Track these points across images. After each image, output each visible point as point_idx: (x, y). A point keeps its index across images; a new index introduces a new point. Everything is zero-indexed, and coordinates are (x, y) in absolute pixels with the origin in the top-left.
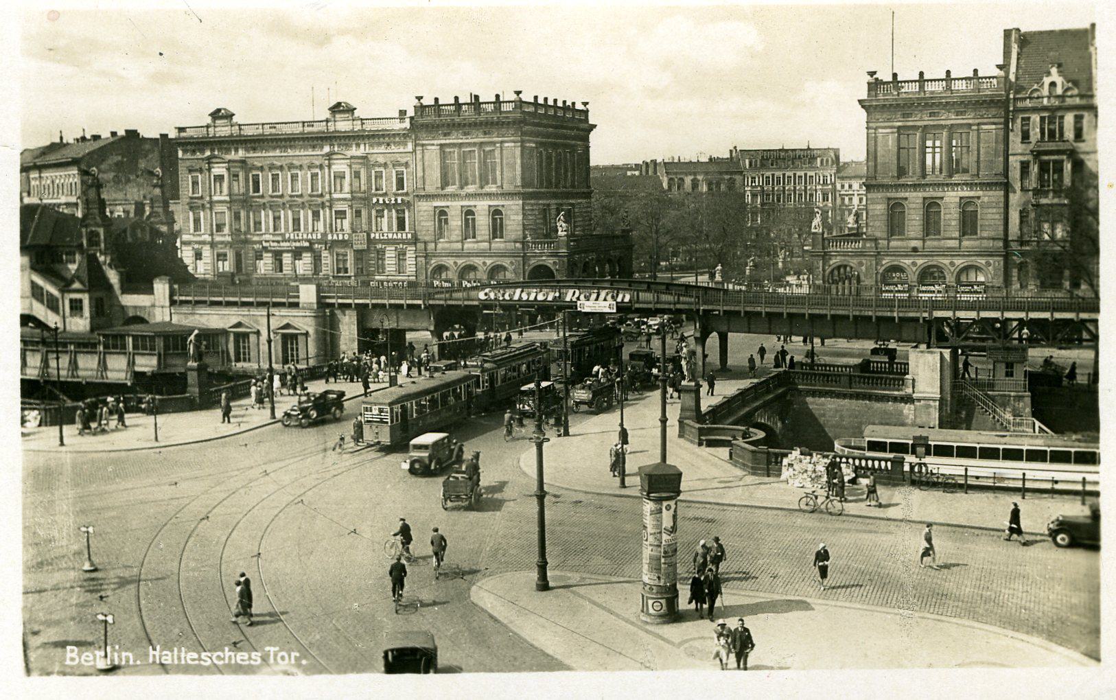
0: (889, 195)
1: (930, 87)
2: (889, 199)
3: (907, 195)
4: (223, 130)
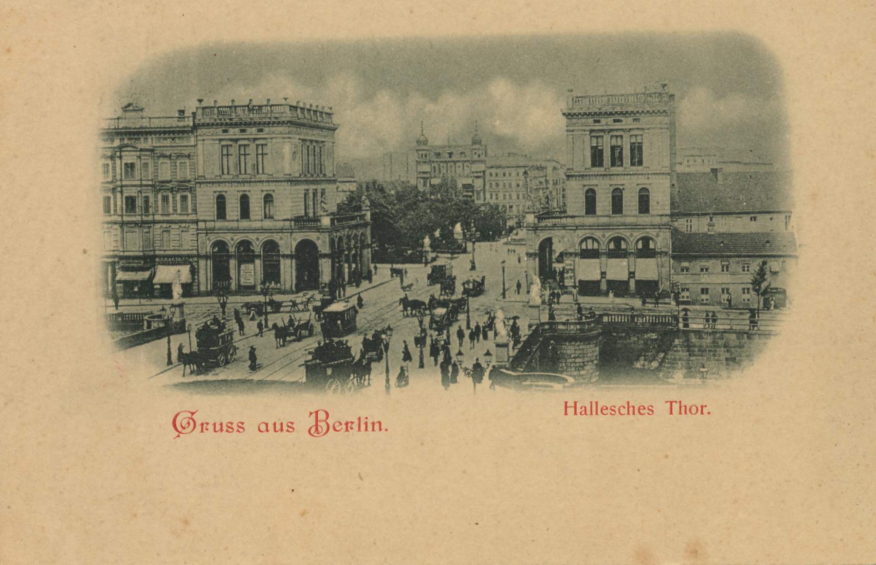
3: (225, 189)
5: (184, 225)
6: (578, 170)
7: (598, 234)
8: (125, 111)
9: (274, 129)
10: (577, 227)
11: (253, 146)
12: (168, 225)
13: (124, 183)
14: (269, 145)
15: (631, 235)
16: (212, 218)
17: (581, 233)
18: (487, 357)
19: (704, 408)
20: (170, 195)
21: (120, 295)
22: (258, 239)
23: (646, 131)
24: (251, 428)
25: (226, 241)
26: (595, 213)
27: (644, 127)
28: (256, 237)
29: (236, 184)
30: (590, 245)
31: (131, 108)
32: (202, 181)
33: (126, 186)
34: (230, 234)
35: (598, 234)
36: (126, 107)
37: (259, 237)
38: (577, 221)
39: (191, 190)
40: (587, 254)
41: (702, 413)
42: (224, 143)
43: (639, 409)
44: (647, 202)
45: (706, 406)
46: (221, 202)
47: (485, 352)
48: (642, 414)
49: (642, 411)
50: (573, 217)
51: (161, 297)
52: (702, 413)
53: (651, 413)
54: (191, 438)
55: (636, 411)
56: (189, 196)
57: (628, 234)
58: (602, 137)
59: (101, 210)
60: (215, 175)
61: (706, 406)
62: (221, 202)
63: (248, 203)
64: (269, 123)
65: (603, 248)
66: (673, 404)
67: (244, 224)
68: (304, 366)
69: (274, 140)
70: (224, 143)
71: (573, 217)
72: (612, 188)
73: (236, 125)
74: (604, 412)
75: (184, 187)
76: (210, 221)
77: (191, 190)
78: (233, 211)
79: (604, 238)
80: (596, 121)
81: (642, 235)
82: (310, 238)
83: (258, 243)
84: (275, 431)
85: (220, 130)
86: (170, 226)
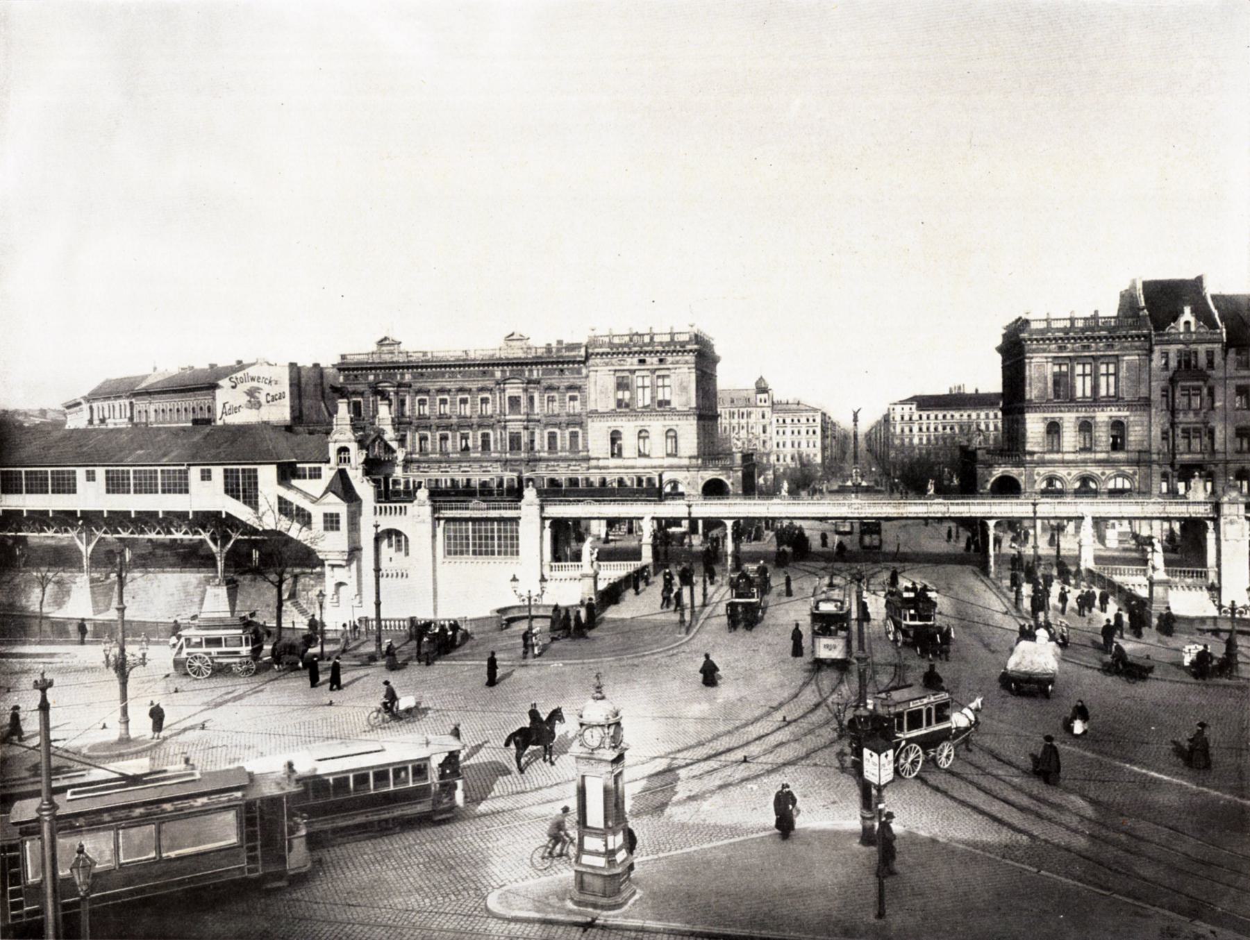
1: (1055, 325)
2: (1046, 418)
4: (517, 353)
8: (382, 345)
9: (678, 358)
13: (508, 418)
14: (673, 376)
16: (605, 456)
18: (514, 583)
20: (471, 434)
21: (1210, 524)
27: (671, 366)
31: (387, 342)
33: (509, 421)
36: (382, 341)
39: (581, 425)
42: (618, 374)
46: (615, 437)
47: (511, 577)
51: (572, 561)
56: (580, 432)
59: (623, 447)
62: (615, 437)
68: (549, 620)
69: (677, 371)
70: (618, 374)
72: (610, 431)
75: (577, 422)
76: (604, 458)
77: (581, 425)
78: (921, 430)
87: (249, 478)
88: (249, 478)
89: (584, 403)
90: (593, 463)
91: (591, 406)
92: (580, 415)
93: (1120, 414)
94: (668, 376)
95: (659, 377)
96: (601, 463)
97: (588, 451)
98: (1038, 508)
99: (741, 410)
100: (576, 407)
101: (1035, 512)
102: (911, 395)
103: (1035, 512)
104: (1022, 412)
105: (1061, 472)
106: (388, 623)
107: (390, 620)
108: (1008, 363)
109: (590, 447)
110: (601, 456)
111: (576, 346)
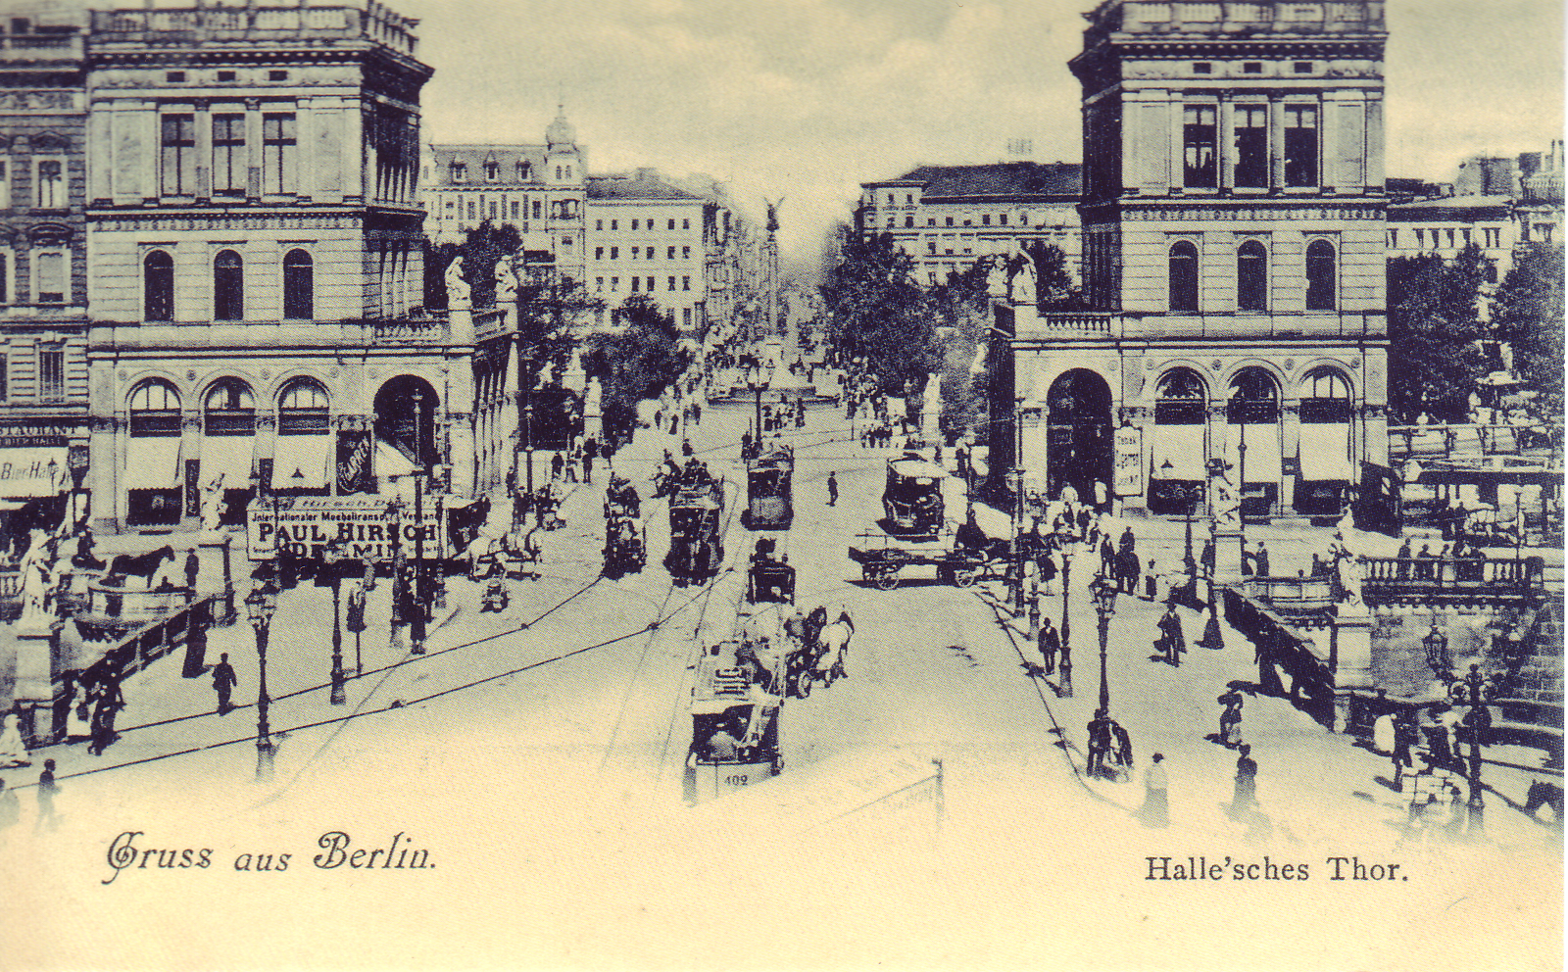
0: (286, 235)
5: (48, 336)
6: (1148, 192)
7: (174, 369)
10: (1149, 342)
11: (255, 117)
12: (59, 337)
15: (1289, 365)
17: (136, 370)
19: (1395, 870)
22: (191, 376)
23: (1326, 96)
24: (222, 861)
25: (1200, 370)
26: (240, 316)
27: (298, 92)
28: (1212, 359)
29: (205, 223)
30: (156, 398)
32: (105, 211)
34: (1283, 351)
35: (174, 369)
37: (272, 369)
38: (1148, 325)
40: (145, 425)
41: (1392, 877)
42: (168, 109)
43: (1284, 870)
44: (308, 290)
45: (1398, 866)
46: (159, 272)
48: (1288, 878)
49: (1288, 874)
50: (1138, 315)
52: (1392, 877)
53: (1238, 868)
54: (131, 874)
55: (1279, 872)
57: (1280, 361)
58: (292, 116)
60: (342, 193)
61: (1398, 866)
62: (159, 272)
63: (308, 274)
64: (307, 56)
65: (191, 404)
66: (1341, 861)
67: (226, 333)
69: (316, 103)
70: (168, 109)
71: (1138, 315)
72: (144, 253)
73: (210, 60)
74: (1288, 874)
79: (194, 378)
80: (274, 76)
81: (1315, 364)
82: (1191, 365)
83: (192, 385)
84: (259, 869)
85: (158, 76)
86: (64, 340)
87: (160, 306)
88: (160, 306)
89: (77, 184)
90: (99, 336)
91: (94, 190)
92: (66, 213)
93: (1322, 225)
94: (292, 116)
95: (268, 117)
96: (121, 336)
97: (86, 304)
98: (1415, 440)
99: (511, 197)
100: (58, 195)
101: (1409, 446)
102: (908, 167)
103: (1409, 446)
104: (1113, 214)
105: (1199, 360)
106: (1386, 565)
107: (1382, 561)
108: (1092, 100)
109: (91, 294)
110: (120, 318)
111: (59, 34)
